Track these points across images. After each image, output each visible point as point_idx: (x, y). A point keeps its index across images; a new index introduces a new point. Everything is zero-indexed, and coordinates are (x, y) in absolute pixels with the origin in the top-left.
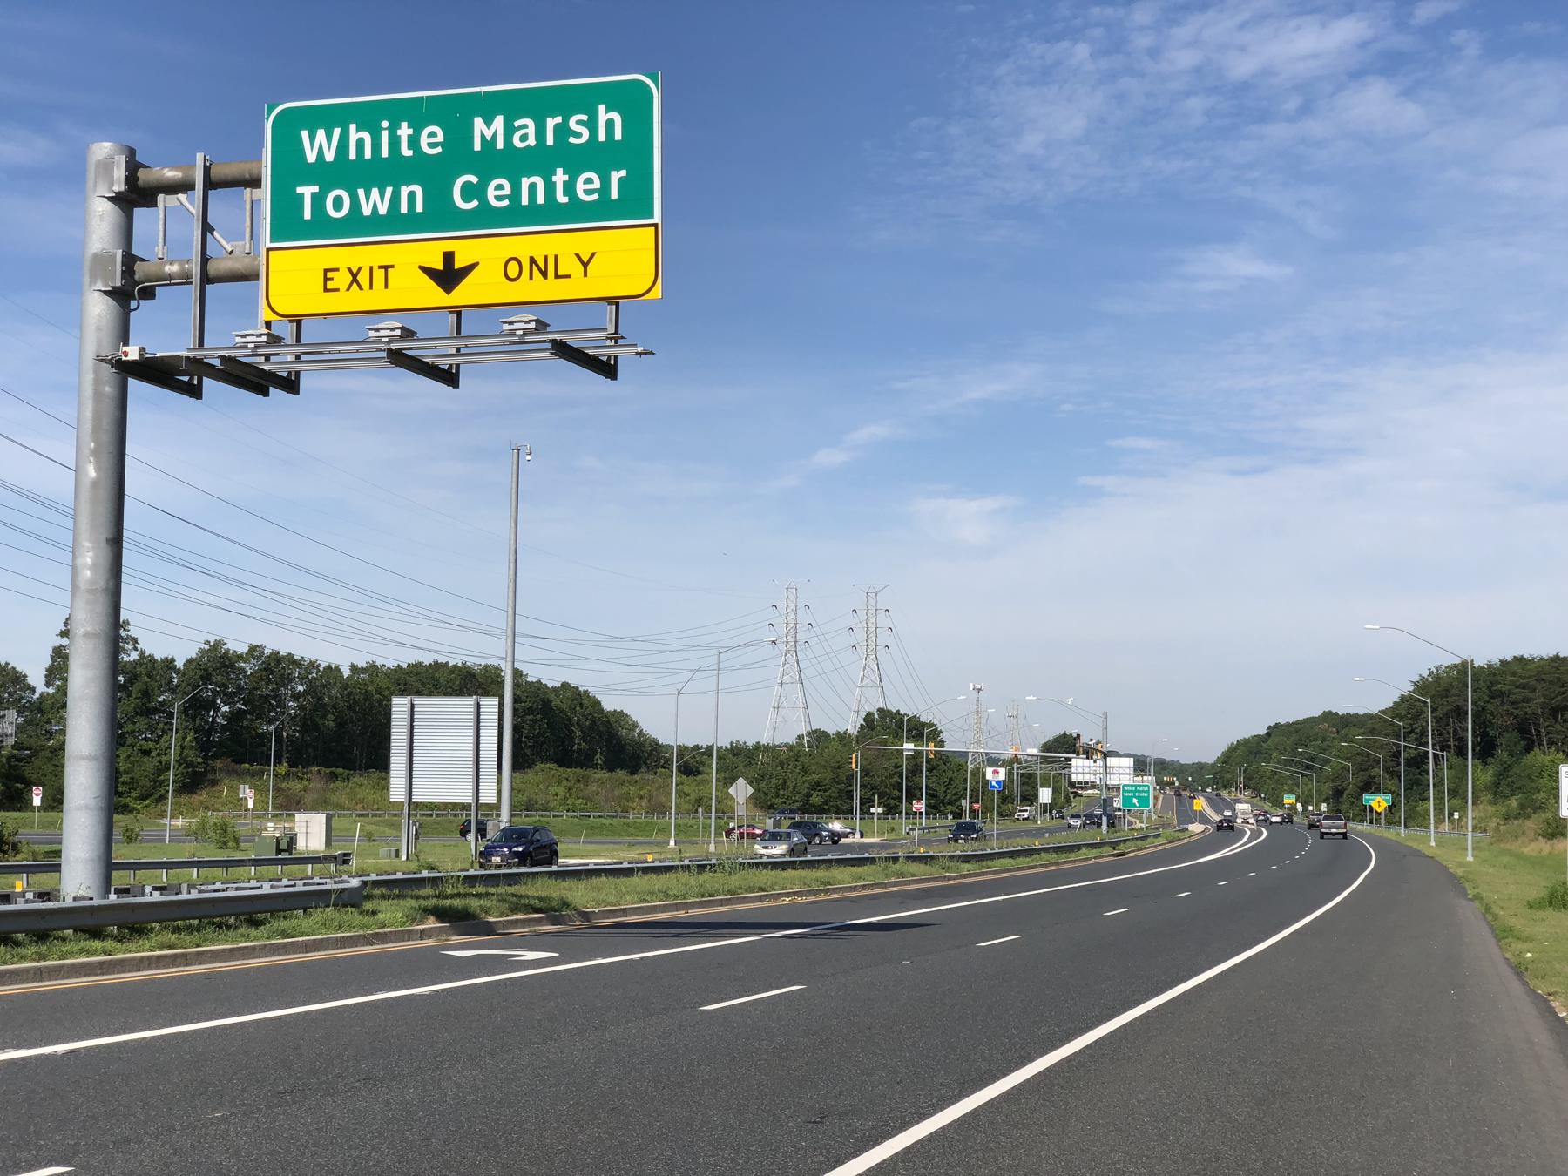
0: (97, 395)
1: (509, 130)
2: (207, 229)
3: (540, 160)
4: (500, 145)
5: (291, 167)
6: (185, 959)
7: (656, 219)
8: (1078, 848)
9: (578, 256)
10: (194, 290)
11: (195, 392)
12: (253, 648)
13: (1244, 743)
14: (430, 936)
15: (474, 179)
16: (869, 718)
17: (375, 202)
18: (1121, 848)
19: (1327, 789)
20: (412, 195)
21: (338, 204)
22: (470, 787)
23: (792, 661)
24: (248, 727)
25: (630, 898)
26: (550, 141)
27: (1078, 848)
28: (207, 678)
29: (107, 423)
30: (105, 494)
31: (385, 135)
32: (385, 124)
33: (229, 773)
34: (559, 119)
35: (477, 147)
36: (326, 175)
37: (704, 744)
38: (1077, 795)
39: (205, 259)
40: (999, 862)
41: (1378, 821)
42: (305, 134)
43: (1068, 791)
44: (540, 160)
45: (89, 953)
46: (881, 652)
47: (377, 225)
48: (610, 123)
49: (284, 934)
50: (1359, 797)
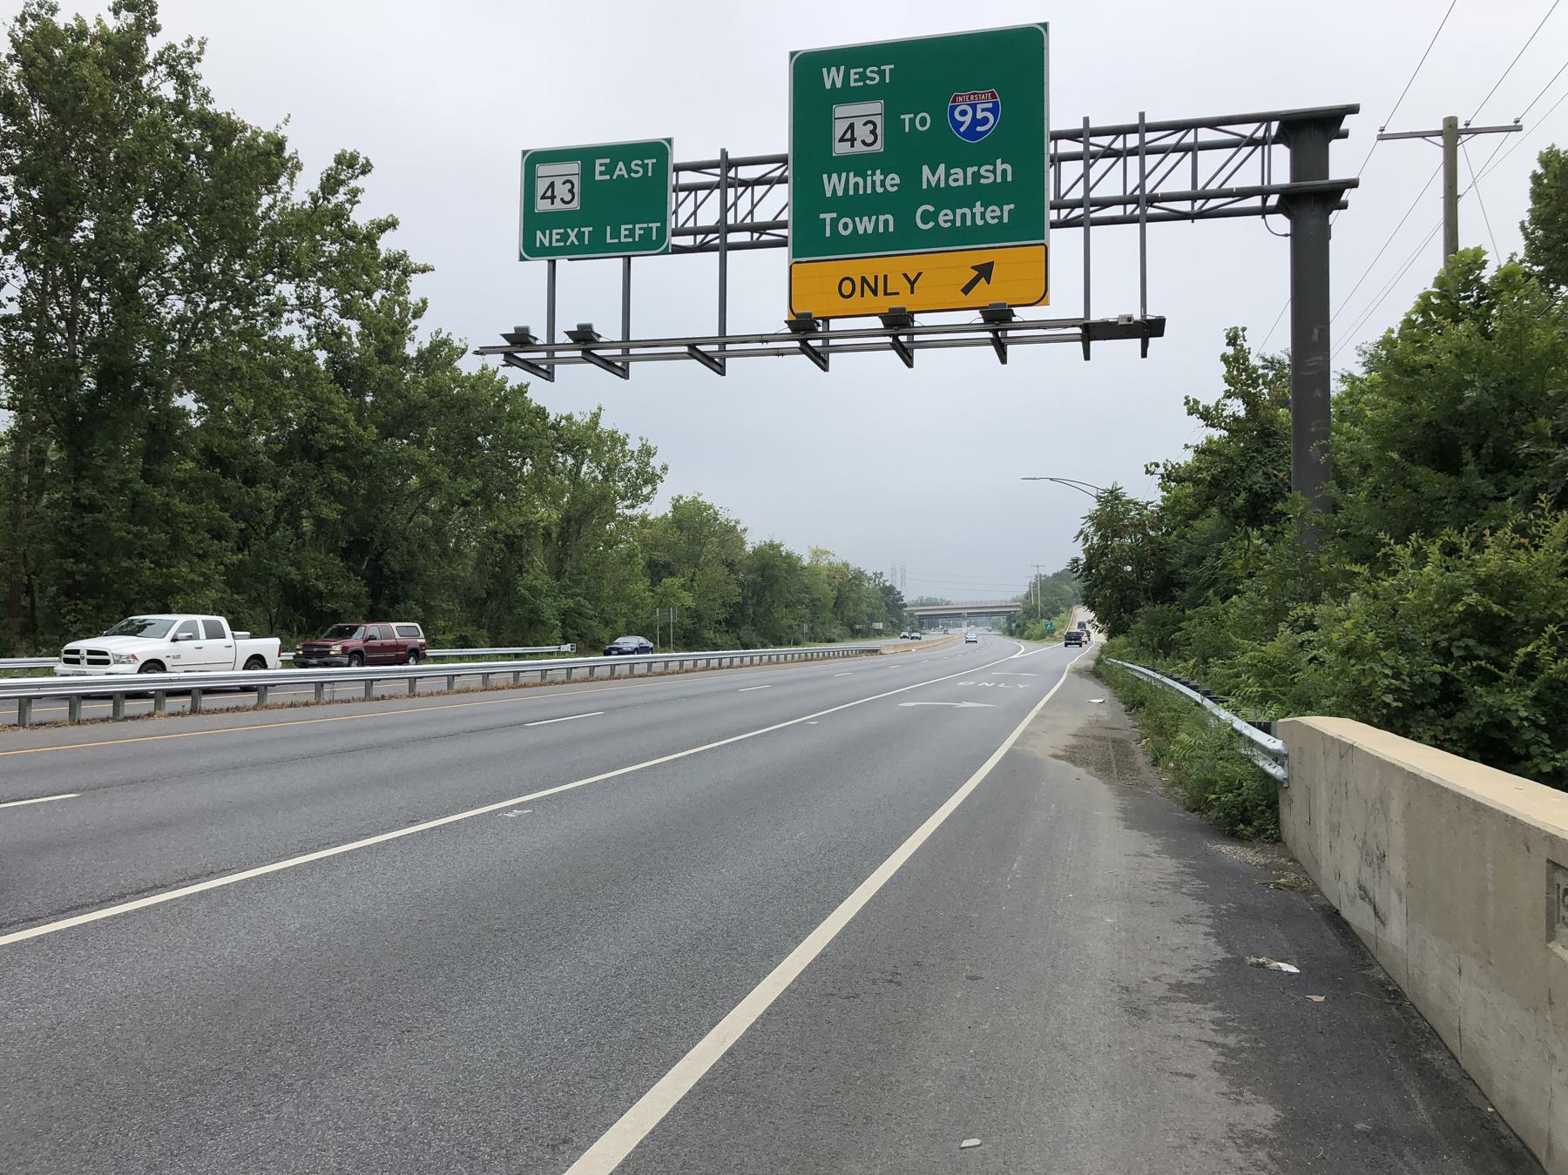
9: (905, 275)
15: (931, 209)
17: (865, 225)
20: (886, 222)
21: (846, 226)
34: (975, 169)
35: (925, 186)
42: (825, 176)
48: (1004, 172)
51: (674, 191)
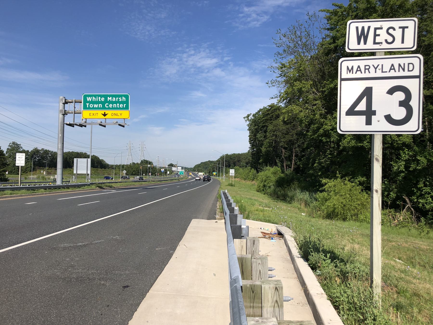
0: (61, 126)
1: (112, 99)
2: (75, 107)
3: (116, 102)
4: (111, 100)
5: (85, 101)
6: (74, 191)
7: (129, 110)
8: (173, 180)
10: (73, 115)
11: (73, 127)
12: (42, 149)
13: (197, 165)
14: (98, 189)
15: (108, 104)
16: (142, 161)
17: (96, 106)
18: (179, 180)
19: (208, 172)
20: (100, 105)
22: (86, 171)
23: (130, 152)
24: (41, 161)
25: (118, 185)
26: (117, 100)
27: (173, 180)
28: (34, 153)
29: (62, 129)
30: (62, 138)
31: (97, 98)
32: (97, 97)
33: (38, 169)
35: (108, 100)
36: (90, 102)
37: (119, 164)
38: (173, 172)
39: (75, 111)
40: (163, 181)
41: (214, 176)
42: (87, 97)
43: (172, 172)
44: (116, 102)
45: (65, 190)
46: (144, 151)
47: (96, 108)
48: (124, 99)
49: (83, 189)
50: (212, 173)
51: (88, 174)
